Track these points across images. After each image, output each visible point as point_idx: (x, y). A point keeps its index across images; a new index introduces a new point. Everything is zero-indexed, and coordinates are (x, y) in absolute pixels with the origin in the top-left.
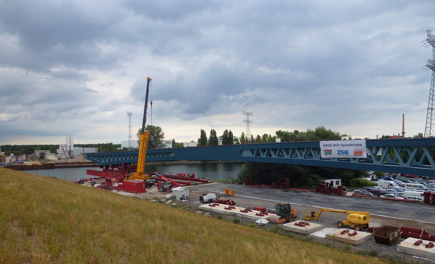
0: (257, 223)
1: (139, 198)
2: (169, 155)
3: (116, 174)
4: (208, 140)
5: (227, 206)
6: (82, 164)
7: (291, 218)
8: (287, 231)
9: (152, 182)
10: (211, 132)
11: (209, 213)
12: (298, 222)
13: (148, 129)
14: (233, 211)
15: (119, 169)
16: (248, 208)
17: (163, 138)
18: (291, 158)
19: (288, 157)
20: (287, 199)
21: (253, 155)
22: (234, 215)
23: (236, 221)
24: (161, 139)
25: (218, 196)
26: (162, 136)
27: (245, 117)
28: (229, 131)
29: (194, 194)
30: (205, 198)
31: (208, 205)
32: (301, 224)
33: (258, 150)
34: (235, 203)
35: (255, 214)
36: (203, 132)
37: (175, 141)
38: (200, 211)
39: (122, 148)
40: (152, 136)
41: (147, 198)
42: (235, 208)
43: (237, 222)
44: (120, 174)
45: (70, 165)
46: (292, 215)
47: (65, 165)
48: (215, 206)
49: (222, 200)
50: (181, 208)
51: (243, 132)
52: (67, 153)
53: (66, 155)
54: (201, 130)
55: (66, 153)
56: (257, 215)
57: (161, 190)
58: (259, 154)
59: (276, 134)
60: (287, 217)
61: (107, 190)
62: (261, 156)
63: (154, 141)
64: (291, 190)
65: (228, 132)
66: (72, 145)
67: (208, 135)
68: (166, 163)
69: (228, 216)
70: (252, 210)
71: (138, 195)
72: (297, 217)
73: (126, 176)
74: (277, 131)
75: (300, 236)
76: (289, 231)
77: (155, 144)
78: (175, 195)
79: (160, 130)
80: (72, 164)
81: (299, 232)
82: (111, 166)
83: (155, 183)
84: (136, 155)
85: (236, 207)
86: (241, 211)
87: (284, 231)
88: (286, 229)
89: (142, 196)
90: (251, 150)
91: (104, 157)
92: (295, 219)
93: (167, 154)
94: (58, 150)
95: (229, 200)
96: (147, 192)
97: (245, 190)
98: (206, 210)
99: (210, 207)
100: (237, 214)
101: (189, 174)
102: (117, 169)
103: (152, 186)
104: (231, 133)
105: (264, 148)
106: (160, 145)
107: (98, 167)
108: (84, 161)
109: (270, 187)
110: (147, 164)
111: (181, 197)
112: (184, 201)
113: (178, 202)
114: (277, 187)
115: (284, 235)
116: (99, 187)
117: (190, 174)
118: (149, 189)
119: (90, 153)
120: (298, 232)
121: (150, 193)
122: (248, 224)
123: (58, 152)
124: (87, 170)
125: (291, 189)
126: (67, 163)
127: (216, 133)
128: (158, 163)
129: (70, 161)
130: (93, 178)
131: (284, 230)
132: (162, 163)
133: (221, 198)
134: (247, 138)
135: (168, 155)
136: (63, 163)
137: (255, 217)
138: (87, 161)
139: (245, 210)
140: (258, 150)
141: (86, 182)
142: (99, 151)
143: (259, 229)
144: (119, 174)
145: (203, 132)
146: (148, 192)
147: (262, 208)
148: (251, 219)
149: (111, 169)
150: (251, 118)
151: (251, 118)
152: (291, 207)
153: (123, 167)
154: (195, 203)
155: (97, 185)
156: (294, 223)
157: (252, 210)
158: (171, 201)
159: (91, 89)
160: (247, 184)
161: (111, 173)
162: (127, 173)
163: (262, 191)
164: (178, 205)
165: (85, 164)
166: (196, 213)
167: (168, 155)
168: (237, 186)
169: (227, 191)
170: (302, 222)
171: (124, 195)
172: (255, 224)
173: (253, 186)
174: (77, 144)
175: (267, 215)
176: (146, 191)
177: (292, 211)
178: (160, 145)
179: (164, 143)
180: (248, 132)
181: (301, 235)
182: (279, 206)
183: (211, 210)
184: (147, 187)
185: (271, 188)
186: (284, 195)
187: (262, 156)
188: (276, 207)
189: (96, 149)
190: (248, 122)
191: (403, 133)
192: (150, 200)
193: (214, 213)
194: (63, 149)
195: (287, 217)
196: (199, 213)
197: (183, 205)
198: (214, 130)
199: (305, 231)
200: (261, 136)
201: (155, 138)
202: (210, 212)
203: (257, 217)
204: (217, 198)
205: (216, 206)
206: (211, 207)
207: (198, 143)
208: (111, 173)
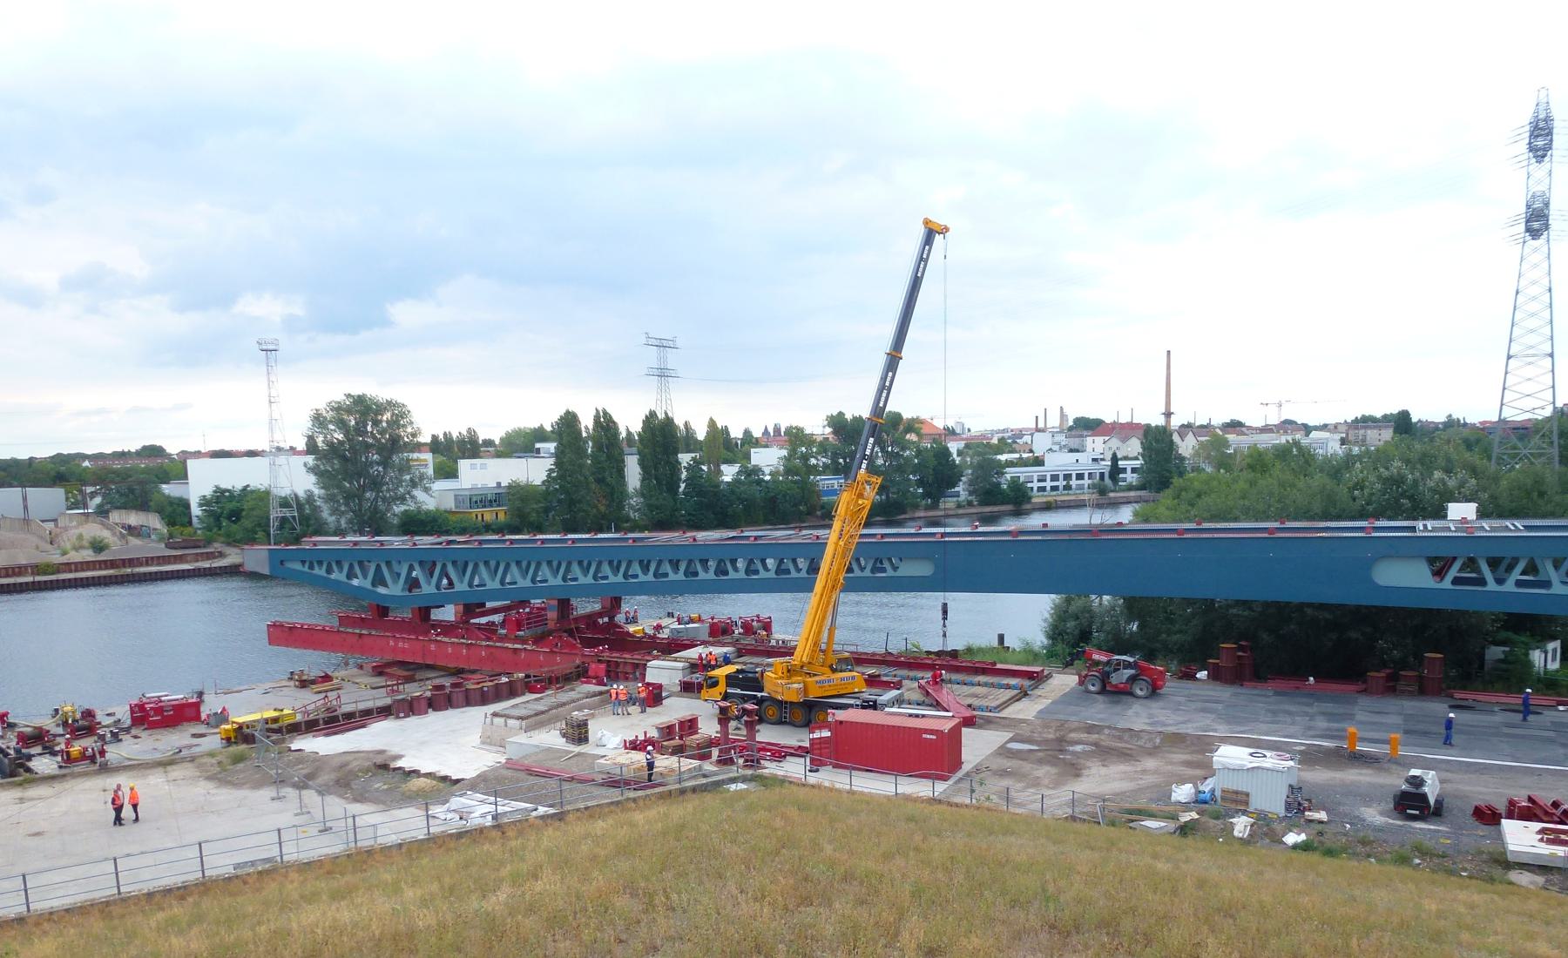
3: (492, 646)
18: (595, 580)
27: (652, 357)
28: (587, 422)
40: (972, 474)
57: (1092, 688)
151: (672, 359)
159: (921, 429)
187: (1492, 586)
190: (663, 374)
191: (1168, 414)
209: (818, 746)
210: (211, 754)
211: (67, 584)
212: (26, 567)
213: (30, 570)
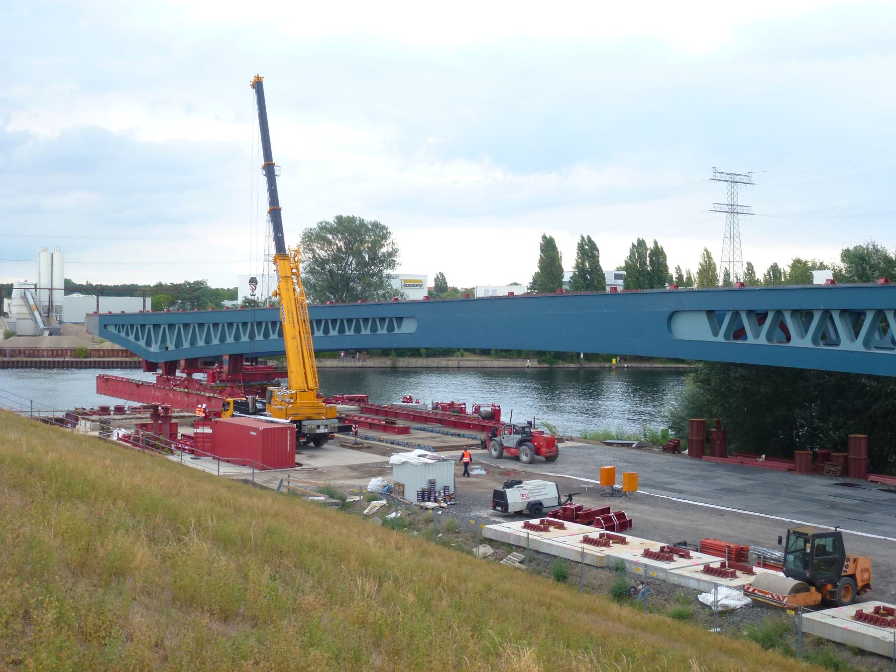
0: (701, 603)
1: (264, 485)
2: (393, 329)
4: (567, 278)
5: (595, 532)
6: (90, 357)
7: (846, 589)
8: (820, 642)
9: (322, 430)
10: (581, 247)
11: (522, 556)
12: (868, 608)
13: (339, 232)
14: (616, 551)
15: (213, 377)
16: (680, 544)
17: (392, 265)
19: (858, 346)
20: (852, 515)
21: (716, 334)
22: (617, 569)
23: (621, 593)
24: (386, 272)
25: (568, 490)
26: (389, 260)
27: (721, 193)
28: (650, 245)
29: (480, 480)
30: (515, 498)
31: (522, 523)
32: (883, 615)
33: (736, 314)
34: (630, 521)
35: (702, 568)
36: (549, 247)
37: (447, 281)
38: (488, 547)
39: (240, 301)
40: (354, 257)
41: (294, 490)
42: (623, 541)
43: (623, 594)
44: (216, 395)
45: (47, 357)
46: (850, 580)
47: (29, 357)
48: (546, 530)
49: (579, 508)
50: (893, 592)
51: (706, 250)
52: (37, 314)
53: (36, 321)
54: (544, 237)
55: (33, 314)
56: (708, 570)
58: (739, 334)
59: (843, 260)
60: (829, 587)
61: (146, 451)
62: (746, 338)
63: (361, 278)
64: (872, 482)
65: (646, 249)
66: (59, 284)
67: (569, 263)
68: (403, 362)
69: (595, 571)
70: (692, 553)
71: (261, 477)
72: (870, 589)
73: (229, 403)
74: (848, 250)
75: (873, 665)
76: (829, 641)
77: (364, 290)
78: (402, 482)
79: (385, 237)
80: (53, 356)
81: (869, 647)
82: (182, 363)
83: (335, 435)
84: (274, 323)
85: (629, 538)
86: (648, 554)
87: (807, 641)
88: (818, 633)
89: (277, 479)
90: (710, 313)
91: (161, 330)
92: (864, 596)
93: (387, 321)
94: (6, 301)
95: (607, 510)
96: (300, 465)
97: (684, 474)
98: (509, 544)
99: (524, 533)
100: (627, 565)
101: (479, 407)
102: (206, 375)
103: (325, 446)
104: (658, 254)
105: (760, 307)
106: (381, 292)
107: (139, 368)
108: (97, 347)
109: (787, 465)
110: (329, 363)
111: (423, 492)
112: (431, 505)
113: (409, 510)
114: (816, 467)
115: (806, 654)
116: (126, 438)
117: (484, 406)
118: (311, 457)
119: (110, 312)
120: (865, 649)
121: (313, 471)
122: (668, 606)
123: (6, 310)
124: (100, 378)
125: (872, 477)
126: (34, 352)
127: (598, 251)
128: (370, 363)
129: (47, 342)
130: (112, 408)
131: (805, 635)
132: (387, 362)
133: (577, 502)
134: (727, 274)
135: (391, 329)
136: (20, 352)
137: (698, 580)
138: (107, 345)
139: (662, 549)
140: (736, 314)
141: (83, 419)
142: (155, 307)
143: (710, 627)
144: (211, 395)
145: (549, 247)
146: (304, 467)
147: (732, 546)
148: (682, 587)
149: (185, 375)
150: (744, 196)
151: (744, 196)
152: (850, 549)
153: (226, 368)
154: (472, 514)
155: (122, 432)
156: (852, 610)
157: (692, 553)
158: (384, 502)
160: (698, 452)
161: (182, 389)
162: (240, 392)
163: (754, 482)
164: (408, 520)
165: (99, 357)
166: (470, 553)
167: (391, 329)
168: (658, 459)
169: (609, 476)
170: (885, 608)
171: (207, 471)
172: (692, 608)
173: (719, 460)
174: (85, 284)
175: (750, 572)
176: (297, 461)
177: (852, 560)
178: (381, 292)
179: (396, 284)
180: (732, 253)
181: (875, 660)
182: (797, 538)
183: (528, 545)
184: (301, 447)
185: (789, 470)
186: (838, 500)
187: (751, 340)
188: (784, 541)
189: (144, 301)
190: (733, 210)
192: (304, 494)
193: (541, 557)
194: (24, 297)
195: (829, 587)
196: (485, 553)
197: (428, 521)
198: (589, 237)
199: (890, 642)
200: (785, 266)
201: (362, 264)
202: (526, 552)
203: (707, 582)
204: (563, 499)
205: (551, 528)
206: (529, 531)
207: (529, 291)
208: (182, 389)
209: (201, 440)
210: (362, 580)
211: (88, 365)
212: (66, 350)
213: (69, 353)
